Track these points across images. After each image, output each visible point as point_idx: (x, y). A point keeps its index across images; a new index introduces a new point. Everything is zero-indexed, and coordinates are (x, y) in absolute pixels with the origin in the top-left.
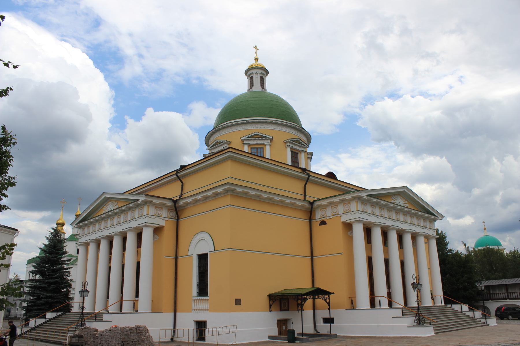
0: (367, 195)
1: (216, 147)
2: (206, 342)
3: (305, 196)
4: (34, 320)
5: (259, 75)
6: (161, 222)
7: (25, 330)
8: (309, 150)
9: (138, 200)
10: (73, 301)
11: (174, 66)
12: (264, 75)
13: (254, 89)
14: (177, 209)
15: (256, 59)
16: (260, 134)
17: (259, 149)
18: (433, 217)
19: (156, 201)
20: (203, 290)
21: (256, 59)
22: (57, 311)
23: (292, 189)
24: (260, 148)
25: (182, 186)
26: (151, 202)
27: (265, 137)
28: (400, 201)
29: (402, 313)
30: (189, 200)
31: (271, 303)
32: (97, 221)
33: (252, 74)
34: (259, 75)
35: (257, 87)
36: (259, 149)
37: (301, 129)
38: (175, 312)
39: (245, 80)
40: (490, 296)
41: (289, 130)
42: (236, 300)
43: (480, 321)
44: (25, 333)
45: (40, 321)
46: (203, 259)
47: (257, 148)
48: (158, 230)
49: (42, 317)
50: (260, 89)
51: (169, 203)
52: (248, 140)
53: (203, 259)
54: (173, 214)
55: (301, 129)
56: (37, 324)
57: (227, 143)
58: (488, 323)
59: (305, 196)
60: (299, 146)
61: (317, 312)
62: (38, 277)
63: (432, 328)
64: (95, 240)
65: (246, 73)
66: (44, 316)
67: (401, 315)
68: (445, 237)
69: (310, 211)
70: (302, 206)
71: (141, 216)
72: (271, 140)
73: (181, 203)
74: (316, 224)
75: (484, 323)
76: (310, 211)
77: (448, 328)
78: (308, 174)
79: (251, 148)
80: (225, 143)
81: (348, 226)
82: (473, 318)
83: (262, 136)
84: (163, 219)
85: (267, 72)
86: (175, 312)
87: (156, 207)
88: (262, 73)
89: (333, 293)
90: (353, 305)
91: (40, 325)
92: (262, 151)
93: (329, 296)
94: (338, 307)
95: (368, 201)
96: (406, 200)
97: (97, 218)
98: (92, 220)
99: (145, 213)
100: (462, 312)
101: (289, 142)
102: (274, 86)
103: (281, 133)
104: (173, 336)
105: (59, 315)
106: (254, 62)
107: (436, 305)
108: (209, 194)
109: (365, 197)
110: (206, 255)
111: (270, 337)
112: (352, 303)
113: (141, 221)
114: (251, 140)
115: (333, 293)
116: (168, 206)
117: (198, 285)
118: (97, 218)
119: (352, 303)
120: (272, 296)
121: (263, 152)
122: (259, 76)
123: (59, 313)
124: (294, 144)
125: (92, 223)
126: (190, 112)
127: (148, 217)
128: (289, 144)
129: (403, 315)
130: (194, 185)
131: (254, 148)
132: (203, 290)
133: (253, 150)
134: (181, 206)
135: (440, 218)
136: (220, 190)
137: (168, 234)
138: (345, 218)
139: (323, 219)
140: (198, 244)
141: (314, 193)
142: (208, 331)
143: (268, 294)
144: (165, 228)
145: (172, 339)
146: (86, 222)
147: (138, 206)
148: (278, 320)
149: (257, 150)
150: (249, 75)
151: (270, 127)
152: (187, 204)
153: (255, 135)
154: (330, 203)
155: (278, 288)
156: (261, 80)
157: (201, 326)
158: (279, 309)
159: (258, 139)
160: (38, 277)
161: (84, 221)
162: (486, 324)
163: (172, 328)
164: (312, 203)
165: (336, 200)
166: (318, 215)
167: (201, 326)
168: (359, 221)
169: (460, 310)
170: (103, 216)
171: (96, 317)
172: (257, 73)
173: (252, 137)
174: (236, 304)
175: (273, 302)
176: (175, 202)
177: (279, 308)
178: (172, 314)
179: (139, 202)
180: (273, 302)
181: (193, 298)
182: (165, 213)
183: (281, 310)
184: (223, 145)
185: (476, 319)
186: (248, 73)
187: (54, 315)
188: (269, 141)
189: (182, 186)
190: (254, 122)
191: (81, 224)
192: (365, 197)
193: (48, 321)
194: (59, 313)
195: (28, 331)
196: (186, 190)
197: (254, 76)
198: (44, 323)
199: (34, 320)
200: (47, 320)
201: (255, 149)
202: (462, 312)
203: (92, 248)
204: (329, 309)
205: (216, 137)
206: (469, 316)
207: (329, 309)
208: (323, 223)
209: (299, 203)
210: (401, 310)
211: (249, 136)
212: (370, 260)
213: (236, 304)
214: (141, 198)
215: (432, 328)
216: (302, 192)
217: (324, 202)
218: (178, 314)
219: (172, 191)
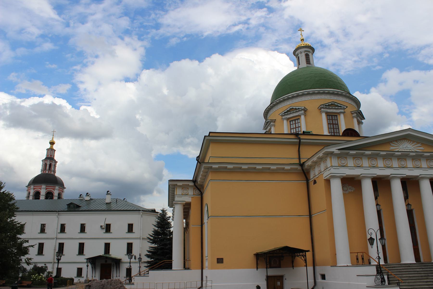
0: (339, 149)
3: (299, 158)
5: (303, 53)
6: (188, 199)
11: (370, 44)
16: (294, 108)
23: (287, 156)
27: (299, 109)
28: (407, 147)
33: (309, 52)
34: (303, 53)
35: (304, 64)
36: (333, 117)
37: (348, 95)
38: (202, 269)
41: (323, 97)
42: (222, 259)
47: (295, 120)
54: (197, 192)
59: (299, 158)
61: (317, 268)
69: (304, 172)
74: (311, 184)
79: (290, 122)
80: (302, 110)
81: (328, 181)
83: (296, 109)
87: (182, 188)
88: (305, 51)
90: (334, 265)
93: (305, 254)
94: (324, 264)
96: (418, 143)
102: (324, 61)
116: (191, 186)
124: (329, 108)
126: (385, 81)
128: (322, 110)
131: (292, 121)
143: (255, 253)
149: (295, 122)
153: (332, 104)
156: (306, 57)
159: (294, 112)
163: (313, 281)
168: (334, 177)
172: (301, 53)
173: (288, 111)
178: (200, 270)
182: (191, 192)
188: (303, 112)
190: (288, 99)
192: (339, 152)
197: (310, 54)
201: (330, 117)
204: (306, 266)
210: (375, 267)
211: (286, 111)
216: (297, 156)
218: (204, 270)
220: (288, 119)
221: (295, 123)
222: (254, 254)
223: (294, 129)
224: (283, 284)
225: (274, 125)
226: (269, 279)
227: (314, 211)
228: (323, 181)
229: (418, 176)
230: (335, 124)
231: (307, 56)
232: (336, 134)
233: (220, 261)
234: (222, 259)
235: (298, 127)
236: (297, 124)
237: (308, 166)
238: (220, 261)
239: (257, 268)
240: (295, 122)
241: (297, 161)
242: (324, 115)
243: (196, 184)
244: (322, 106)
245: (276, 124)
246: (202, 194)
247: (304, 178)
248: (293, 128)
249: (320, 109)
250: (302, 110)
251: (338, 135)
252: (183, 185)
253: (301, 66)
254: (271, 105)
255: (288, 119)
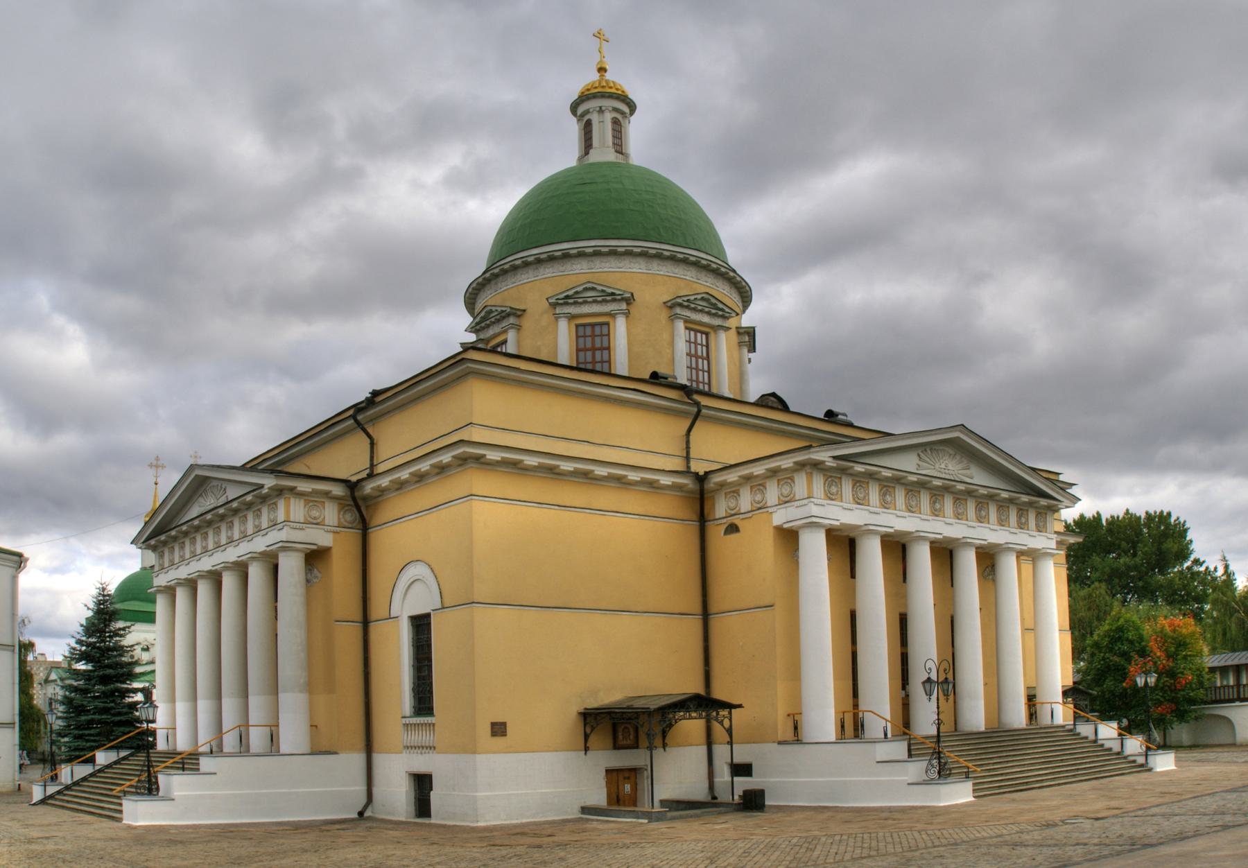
0: (834, 457)
1: (488, 326)
2: (433, 820)
3: (687, 458)
4: (69, 769)
6: (322, 538)
7: (52, 789)
8: (746, 320)
9: (262, 486)
10: (1056, 516)
12: (623, 113)
13: (595, 157)
14: (360, 505)
15: (602, 70)
17: (597, 329)
18: (1044, 502)
19: (304, 486)
20: (423, 702)
21: (602, 70)
22: (117, 748)
24: (601, 324)
25: (372, 444)
26: (292, 489)
27: (613, 294)
29: (909, 750)
30: (384, 482)
31: (588, 731)
32: (186, 534)
33: (587, 112)
38: (369, 749)
39: (573, 128)
40: (1239, 692)
42: (504, 724)
43: (1134, 761)
44: (51, 797)
45: (82, 771)
46: (421, 624)
47: (593, 325)
48: (315, 558)
49: (86, 761)
50: (611, 156)
51: (338, 490)
52: (567, 304)
53: (421, 624)
55: (732, 274)
56: (77, 777)
57: (514, 315)
58: (1151, 764)
60: (709, 313)
62: (81, 666)
63: (968, 786)
64: (210, 572)
65: (574, 108)
66: (92, 760)
67: (905, 756)
68: (1186, 531)
69: (699, 495)
70: (675, 487)
71: (274, 524)
72: (629, 301)
73: (369, 488)
74: (716, 533)
75: (1142, 765)
76: (699, 495)
77: (1000, 787)
78: (697, 404)
79: (577, 326)
80: (509, 315)
81: (789, 538)
82: (1118, 753)
84: (326, 527)
85: (632, 107)
86: (369, 749)
88: (616, 110)
89: (740, 706)
90: (796, 734)
91: (84, 779)
92: (605, 331)
93: (730, 713)
95: (843, 471)
97: (184, 528)
98: (173, 533)
99: (281, 516)
100: (1095, 741)
101: (680, 305)
102: (644, 144)
103: (651, 283)
104: (366, 807)
105: (124, 758)
106: (595, 76)
107: (1045, 720)
108: (424, 466)
109: (831, 463)
110: (428, 616)
111: (585, 810)
112: (796, 728)
113: (274, 537)
114: (575, 303)
115: (740, 706)
117: (413, 690)
118: (184, 528)
119: (796, 728)
120: (590, 714)
121: (608, 335)
122: (608, 117)
123: (123, 754)
125: (175, 539)
127: (298, 523)
128: (678, 310)
129: (910, 755)
130: (400, 438)
131: (584, 325)
132: (423, 702)
133: (581, 329)
134: (366, 498)
135: (1066, 502)
136: (446, 458)
137: (342, 569)
138: (781, 517)
139: (731, 520)
140: (408, 594)
141: (717, 447)
142: (435, 796)
144: (336, 556)
145: (361, 814)
146: (163, 538)
147: (264, 499)
148: (608, 771)
149: (593, 331)
150: (583, 115)
151: (638, 267)
152: (382, 491)
153: (586, 289)
154: (774, 472)
155: (609, 697)
157: (422, 783)
158: (611, 745)
160: (81, 666)
161: (162, 533)
162: (1145, 768)
163: (363, 788)
164: (701, 479)
165: (787, 463)
166: (721, 508)
167: (422, 783)
169: (1092, 737)
170: (196, 522)
171: (183, 763)
174: (504, 734)
175: (593, 729)
176: (352, 486)
177: (610, 742)
179: (265, 491)
180: (593, 729)
181: (404, 721)
182: (331, 513)
183: (616, 746)
184: (504, 318)
185: (1125, 758)
186: (580, 110)
187: (112, 756)
189: (372, 444)
191: (153, 542)
193: (100, 771)
194: (123, 754)
195: (59, 792)
196: (383, 451)
197: (595, 118)
198: (91, 775)
199: (69, 769)
200: (97, 768)
202: (1095, 741)
203: (204, 589)
204: (731, 743)
205: (488, 298)
206: (1110, 749)
207: (731, 743)
208: (733, 529)
209: (666, 480)
212: (851, 623)
213: (504, 734)
214: (269, 482)
215: (968, 786)
216: (679, 449)
217: (732, 477)
218: (378, 758)
219: (346, 459)
220: (572, 317)
221: (593, 336)
222: (580, 713)
223: (589, 354)
224: (639, 792)
225: (518, 328)
226: (613, 775)
227: (713, 607)
228: (772, 531)
229: (860, 526)
230: (602, 349)
231: (616, 122)
232: (598, 367)
233: (499, 729)
234: (504, 724)
235: (602, 349)
236: (598, 340)
237: (715, 483)
238: (499, 729)
239: (586, 749)
240: (593, 331)
241: (677, 464)
242: (680, 325)
243: (357, 494)
244: (679, 300)
245: (527, 323)
246: (364, 527)
247: (691, 513)
248: (585, 350)
249: (671, 305)
250: (623, 299)
251: (606, 370)
252: (315, 493)
253: (595, 157)
254: (488, 275)
255: (572, 317)
